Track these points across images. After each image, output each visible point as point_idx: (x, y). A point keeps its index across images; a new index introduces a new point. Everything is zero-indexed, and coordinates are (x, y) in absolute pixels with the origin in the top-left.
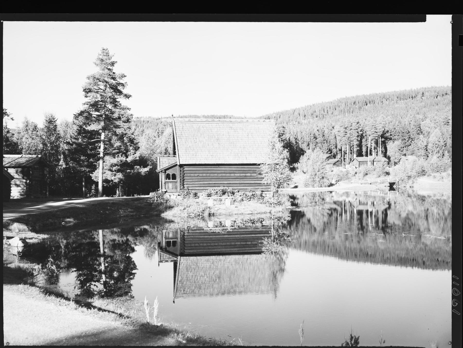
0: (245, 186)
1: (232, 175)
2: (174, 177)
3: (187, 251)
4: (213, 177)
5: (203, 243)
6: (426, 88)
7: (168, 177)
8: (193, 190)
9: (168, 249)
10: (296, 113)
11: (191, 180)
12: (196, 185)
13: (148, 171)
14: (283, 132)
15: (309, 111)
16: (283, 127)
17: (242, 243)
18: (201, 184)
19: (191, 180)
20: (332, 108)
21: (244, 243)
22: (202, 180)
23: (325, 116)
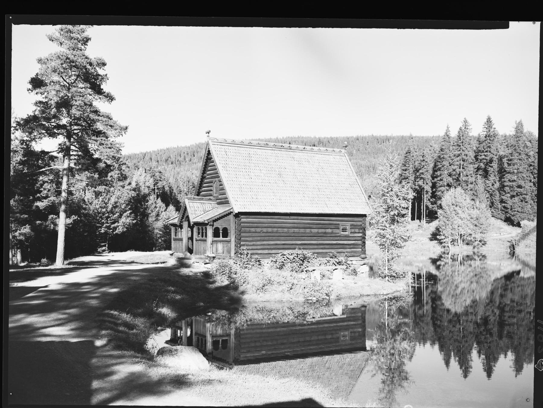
0: (325, 249)
1: (308, 230)
2: (226, 233)
3: (242, 357)
4: (282, 234)
5: (266, 341)
6: (292, 138)
7: (216, 234)
8: (256, 254)
9: (215, 353)
10: (147, 158)
11: (251, 239)
12: (259, 247)
13: (71, 224)
14: (159, 179)
15: (162, 156)
16: (160, 172)
17: (320, 337)
18: (264, 245)
19: (251, 239)
20: (189, 154)
21: (323, 337)
22: (266, 238)
23: (182, 163)
